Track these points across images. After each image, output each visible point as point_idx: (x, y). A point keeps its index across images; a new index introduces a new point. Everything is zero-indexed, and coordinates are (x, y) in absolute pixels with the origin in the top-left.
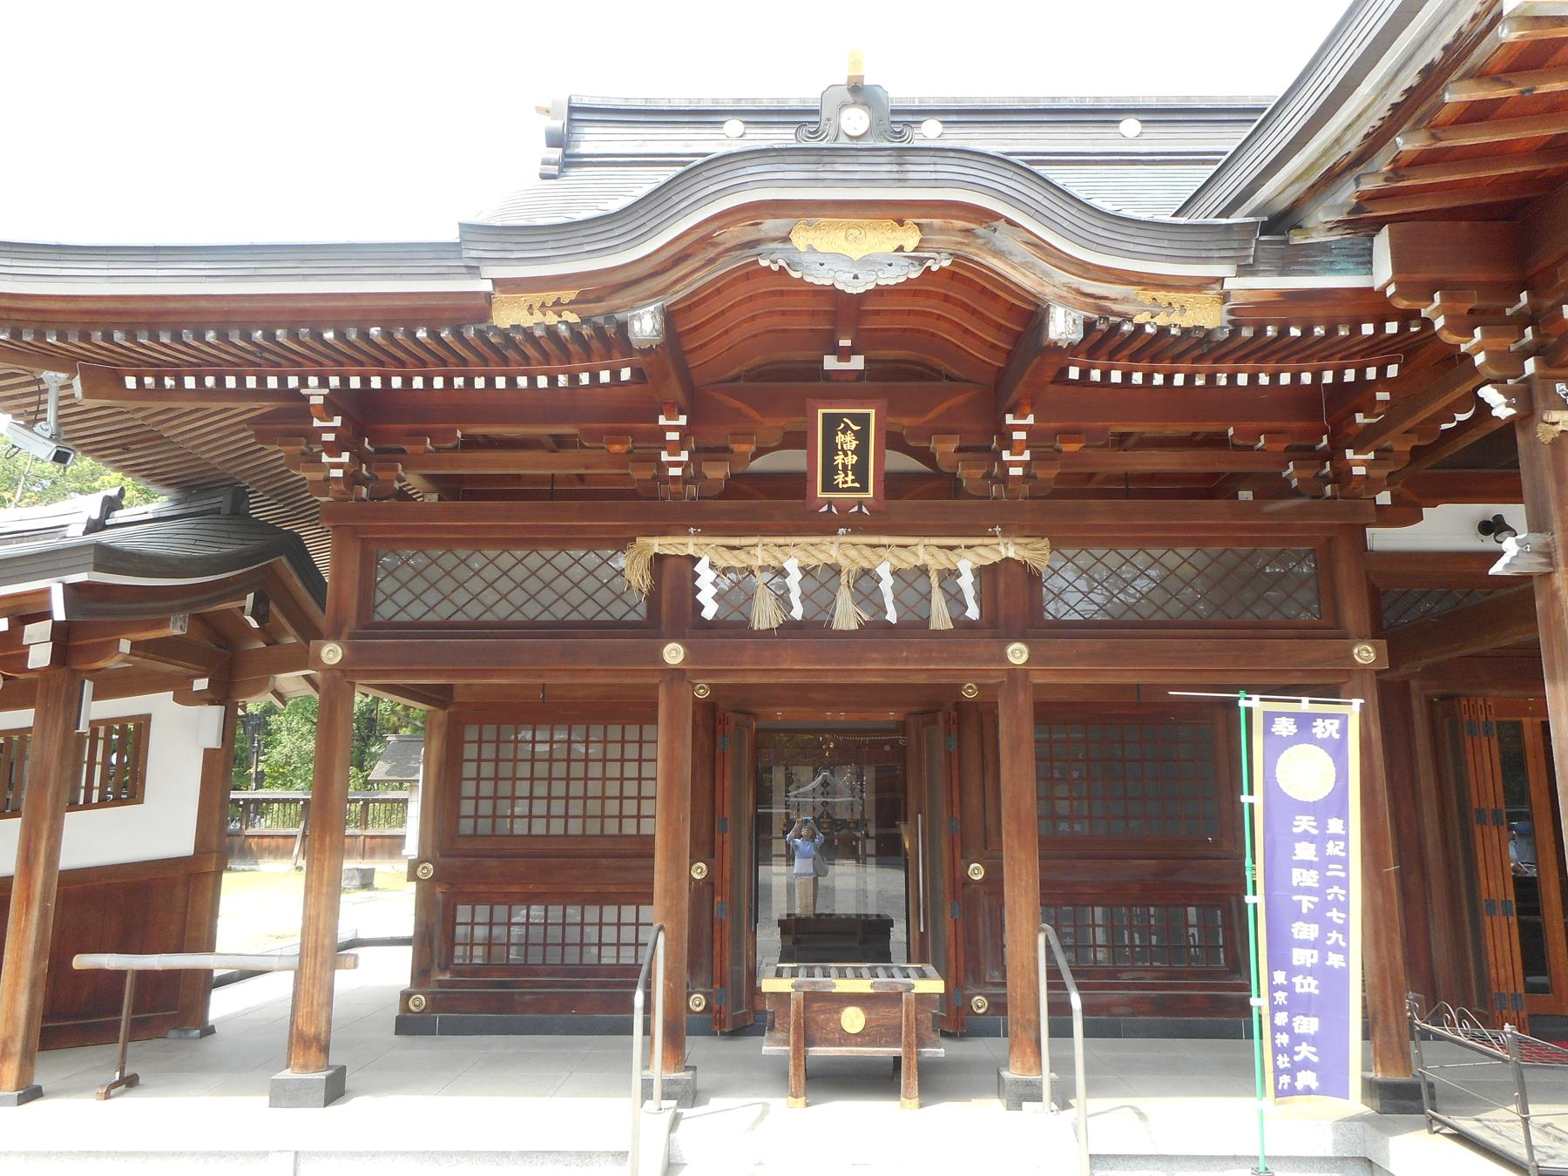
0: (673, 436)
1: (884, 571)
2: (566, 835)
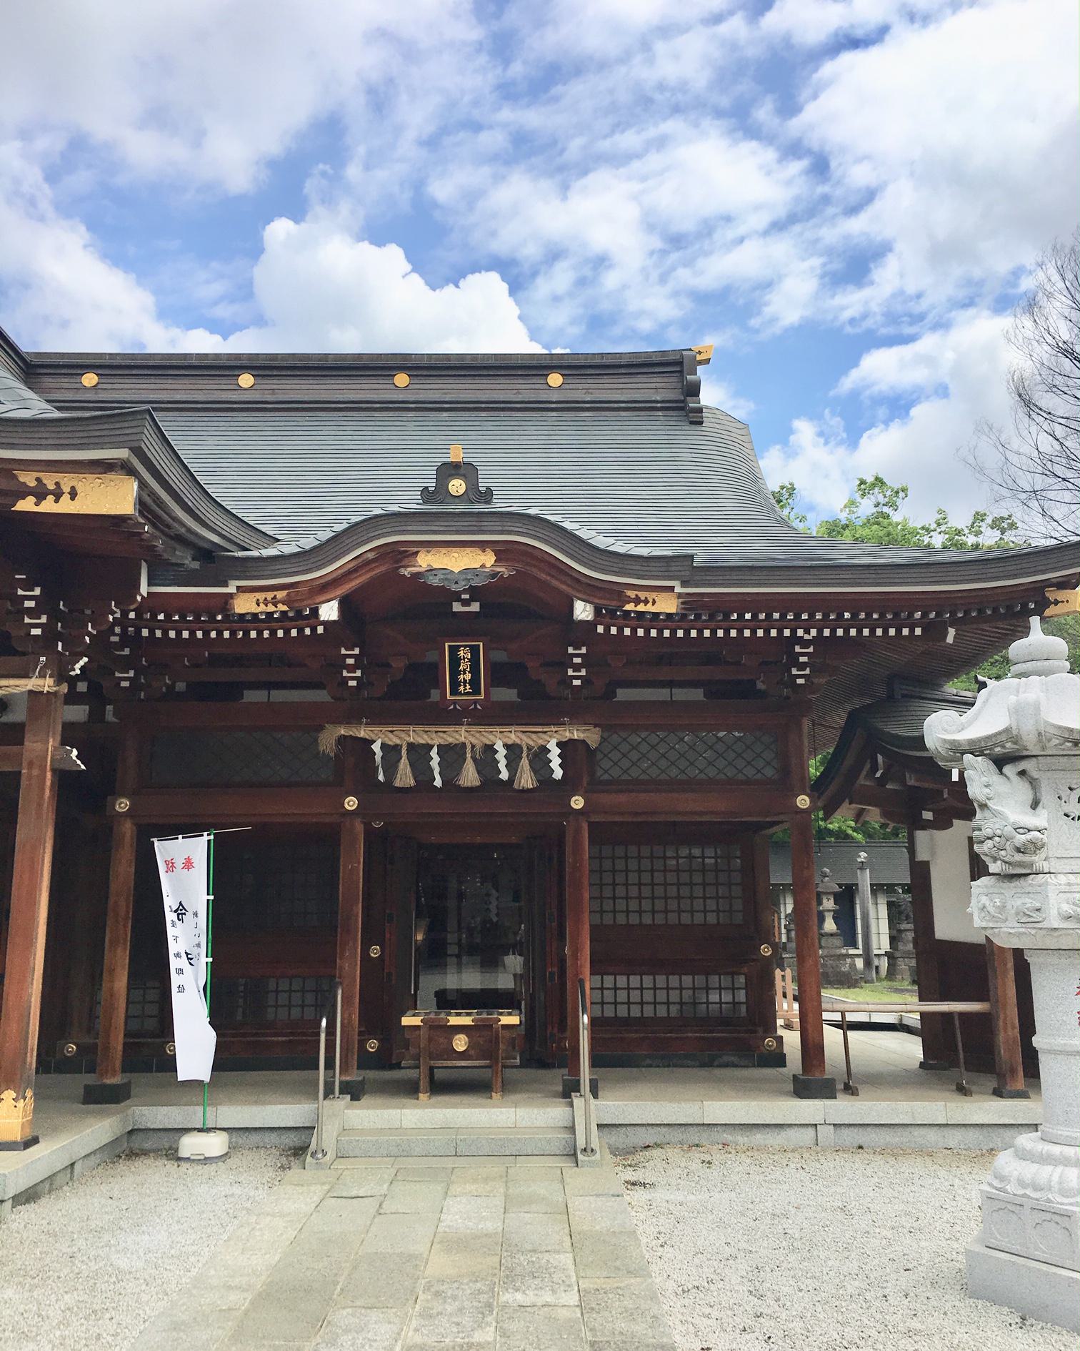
0: (350, 661)
1: (499, 746)
2: (628, 976)
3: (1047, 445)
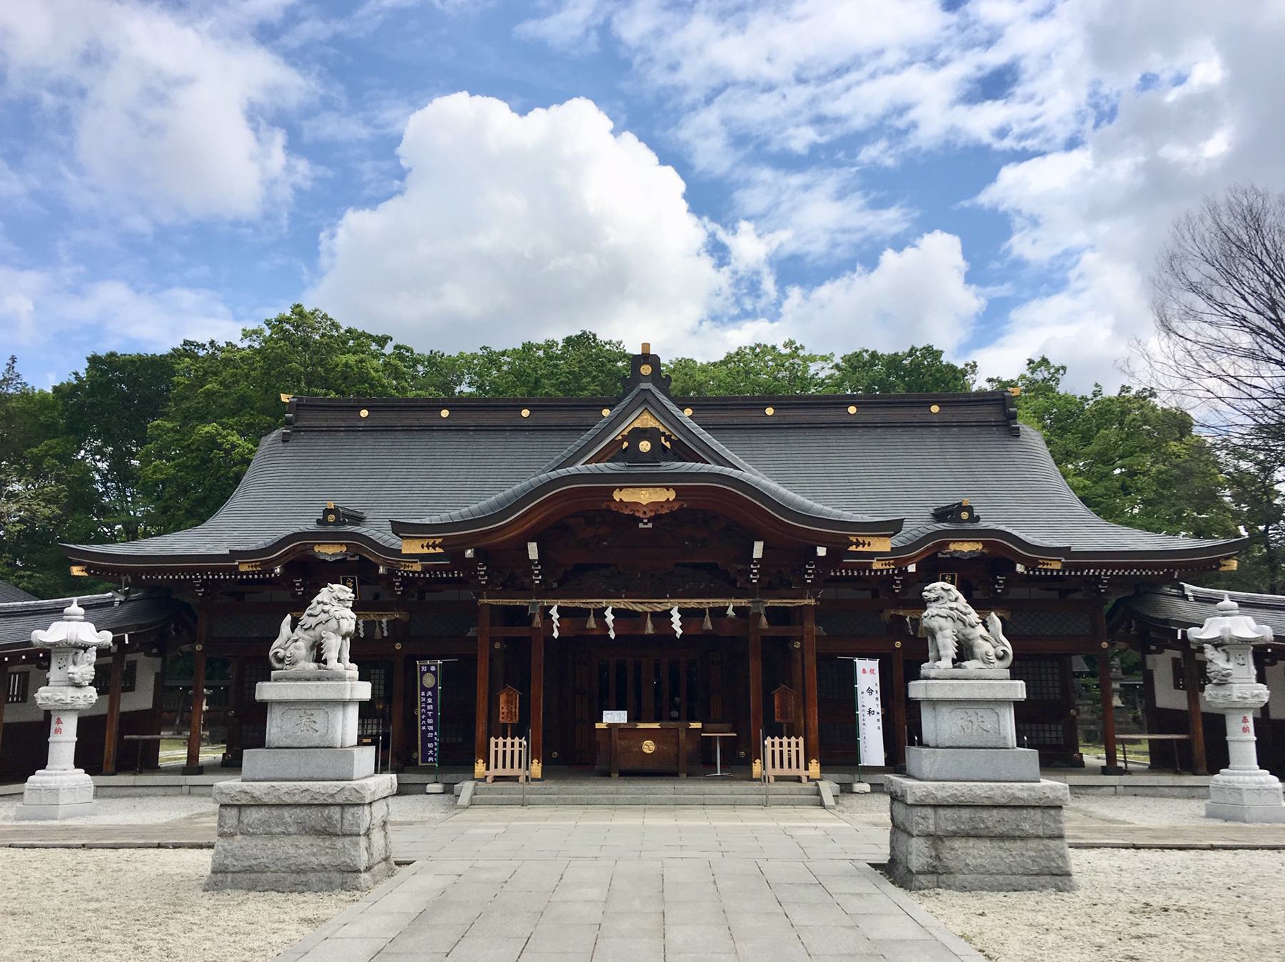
3: (1180, 354)
